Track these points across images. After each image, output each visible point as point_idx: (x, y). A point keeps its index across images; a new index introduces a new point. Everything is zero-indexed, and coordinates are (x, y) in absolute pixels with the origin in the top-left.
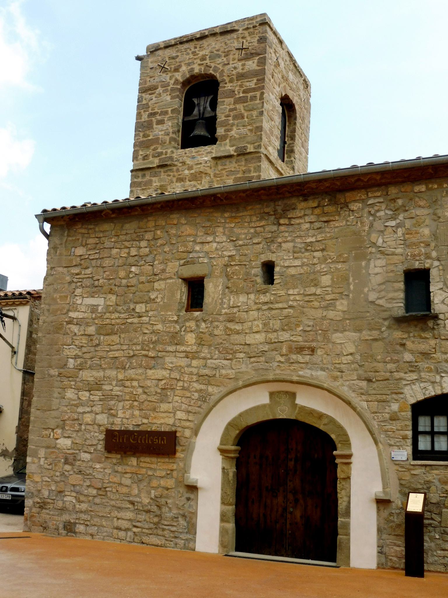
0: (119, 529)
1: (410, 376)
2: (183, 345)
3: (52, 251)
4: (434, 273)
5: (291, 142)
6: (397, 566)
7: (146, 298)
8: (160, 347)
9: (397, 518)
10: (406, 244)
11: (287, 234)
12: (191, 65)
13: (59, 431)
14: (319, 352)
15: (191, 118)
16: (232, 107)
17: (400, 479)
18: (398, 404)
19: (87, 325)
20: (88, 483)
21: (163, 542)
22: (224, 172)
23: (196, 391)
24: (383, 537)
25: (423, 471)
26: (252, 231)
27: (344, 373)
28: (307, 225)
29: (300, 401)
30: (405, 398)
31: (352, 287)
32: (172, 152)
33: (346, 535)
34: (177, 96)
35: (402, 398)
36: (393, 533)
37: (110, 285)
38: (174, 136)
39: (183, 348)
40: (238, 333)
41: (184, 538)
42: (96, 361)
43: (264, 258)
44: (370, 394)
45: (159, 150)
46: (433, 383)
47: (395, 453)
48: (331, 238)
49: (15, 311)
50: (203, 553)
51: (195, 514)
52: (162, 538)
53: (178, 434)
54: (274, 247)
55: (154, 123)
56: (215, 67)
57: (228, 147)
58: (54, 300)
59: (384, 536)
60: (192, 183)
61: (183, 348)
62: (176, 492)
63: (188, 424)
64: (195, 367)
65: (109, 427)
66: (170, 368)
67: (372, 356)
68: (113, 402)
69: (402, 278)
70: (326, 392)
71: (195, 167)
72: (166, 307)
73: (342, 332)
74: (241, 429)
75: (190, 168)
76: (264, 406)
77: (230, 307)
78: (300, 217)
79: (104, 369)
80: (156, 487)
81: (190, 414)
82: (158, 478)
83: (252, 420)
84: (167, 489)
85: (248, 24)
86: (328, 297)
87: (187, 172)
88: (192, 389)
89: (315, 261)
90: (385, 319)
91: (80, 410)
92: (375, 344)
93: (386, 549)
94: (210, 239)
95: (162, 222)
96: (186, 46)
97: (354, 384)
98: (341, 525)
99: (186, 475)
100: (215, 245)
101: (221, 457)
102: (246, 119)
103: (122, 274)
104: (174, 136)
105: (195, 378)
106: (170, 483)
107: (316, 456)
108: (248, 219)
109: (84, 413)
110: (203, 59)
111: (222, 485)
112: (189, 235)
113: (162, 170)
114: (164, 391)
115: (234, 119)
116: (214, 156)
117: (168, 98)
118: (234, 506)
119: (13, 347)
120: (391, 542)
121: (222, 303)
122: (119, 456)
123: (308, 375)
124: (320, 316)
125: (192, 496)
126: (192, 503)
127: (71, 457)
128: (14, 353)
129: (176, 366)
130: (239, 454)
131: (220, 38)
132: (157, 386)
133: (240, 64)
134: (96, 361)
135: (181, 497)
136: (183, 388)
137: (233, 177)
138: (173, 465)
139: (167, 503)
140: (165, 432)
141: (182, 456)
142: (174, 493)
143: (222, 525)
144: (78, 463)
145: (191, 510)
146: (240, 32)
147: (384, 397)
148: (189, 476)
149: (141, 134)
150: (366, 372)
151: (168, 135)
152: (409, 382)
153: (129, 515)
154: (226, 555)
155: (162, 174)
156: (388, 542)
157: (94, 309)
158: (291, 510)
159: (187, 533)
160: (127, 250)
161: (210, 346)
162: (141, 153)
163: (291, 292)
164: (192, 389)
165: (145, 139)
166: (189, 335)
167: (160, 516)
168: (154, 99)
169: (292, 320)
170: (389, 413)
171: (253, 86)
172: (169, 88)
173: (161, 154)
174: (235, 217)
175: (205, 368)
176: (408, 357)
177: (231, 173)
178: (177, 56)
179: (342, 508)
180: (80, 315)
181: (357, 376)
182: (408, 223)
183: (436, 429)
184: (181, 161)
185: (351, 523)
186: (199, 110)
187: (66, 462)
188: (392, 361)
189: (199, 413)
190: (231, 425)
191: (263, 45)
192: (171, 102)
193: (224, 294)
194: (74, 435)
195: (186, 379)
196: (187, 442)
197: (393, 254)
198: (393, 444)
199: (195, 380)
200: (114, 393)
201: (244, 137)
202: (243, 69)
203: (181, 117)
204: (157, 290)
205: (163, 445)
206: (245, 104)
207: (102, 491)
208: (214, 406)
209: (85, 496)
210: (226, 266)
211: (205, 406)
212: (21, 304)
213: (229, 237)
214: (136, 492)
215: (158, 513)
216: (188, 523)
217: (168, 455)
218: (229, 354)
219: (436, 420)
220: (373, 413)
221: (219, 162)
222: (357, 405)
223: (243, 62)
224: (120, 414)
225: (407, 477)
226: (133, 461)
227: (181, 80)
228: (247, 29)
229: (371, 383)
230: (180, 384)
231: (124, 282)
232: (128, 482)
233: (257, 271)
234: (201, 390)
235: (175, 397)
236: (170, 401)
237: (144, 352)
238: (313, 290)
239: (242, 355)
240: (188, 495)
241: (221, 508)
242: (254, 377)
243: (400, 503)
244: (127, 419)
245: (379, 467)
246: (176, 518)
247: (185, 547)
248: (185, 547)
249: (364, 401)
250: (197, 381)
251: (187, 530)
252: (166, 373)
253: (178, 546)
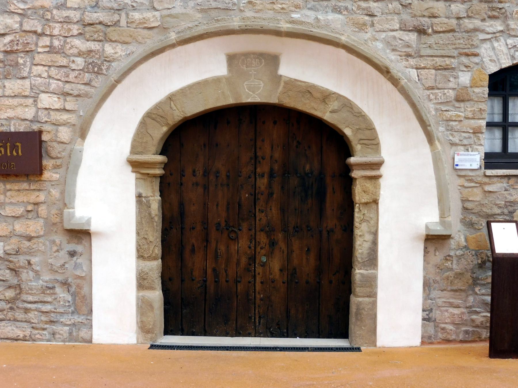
1: (491, 26)
6: (454, 337)
9: (458, 264)
18: (470, 73)
21: (28, 332)
23: (80, 54)
24: (432, 296)
25: (505, 185)
27: (376, 18)
29: (286, 70)
33: (369, 296)
35: (477, 64)
36: (449, 288)
41: (69, 323)
44: (421, 56)
47: (460, 157)
50: (109, 346)
51: (88, 279)
52: (25, 325)
53: (45, 137)
59: (435, 294)
62: (48, 243)
63: (65, 117)
64: (75, 9)
66: (20, 11)
70: (343, 52)
74: (171, 123)
76: (217, 80)
80: (6, 236)
81: (68, 98)
82: (10, 220)
83: (194, 107)
84: (30, 238)
88: (71, 51)
93: (436, 314)
97: (394, 38)
98: (361, 281)
99: (66, 211)
101: (133, 176)
105: (75, 29)
106: (35, 227)
107: (308, 167)
111: (137, 226)
114: (11, 57)
118: (160, 260)
120: (445, 302)
123: (311, 20)
125: (79, 248)
126: (79, 261)
129: (34, 8)
130: (164, 169)
135: (58, 251)
136: (51, 50)
138: (37, 193)
139: (29, 263)
141: (56, 176)
142: (44, 244)
143: (141, 294)
145: (78, 273)
147: (448, 61)
148: (74, 213)
150: (415, 16)
152: (489, 36)
154: (152, 347)
156: (440, 302)
158: (264, 259)
159: (73, 313)
164: (71, 51)
167: (18, 287)
170: (454, 89)
175: (96, 9)
179: (362, 253)
181: (400, 23)
185: (379, 276)
189: (87, 95)
190: (151, 116)
195: (56, 32)
196: (64, 150)
198: (457, 141)
199: (75, 32)
208: (118, 81)
215: (15, 281)
216: (74, 295)
217: (27, 175)
220: (428, 89)
222: (400, 74)
225: (477, 195)
229: (423, 37)
230: (46, 41)
234: (91, 51)
235: (35, 68)
236: (25, 74)
240: (72, 247)
241: (138, 266)
243: (463, 239)
245: (434, 182)
246: (50, 288)
247: (71, 338)
248: (71, 338)
249: (413, 68)
250: (80, 34)
251: (72, 308)
252: (13, 22)
253: (57, 336)
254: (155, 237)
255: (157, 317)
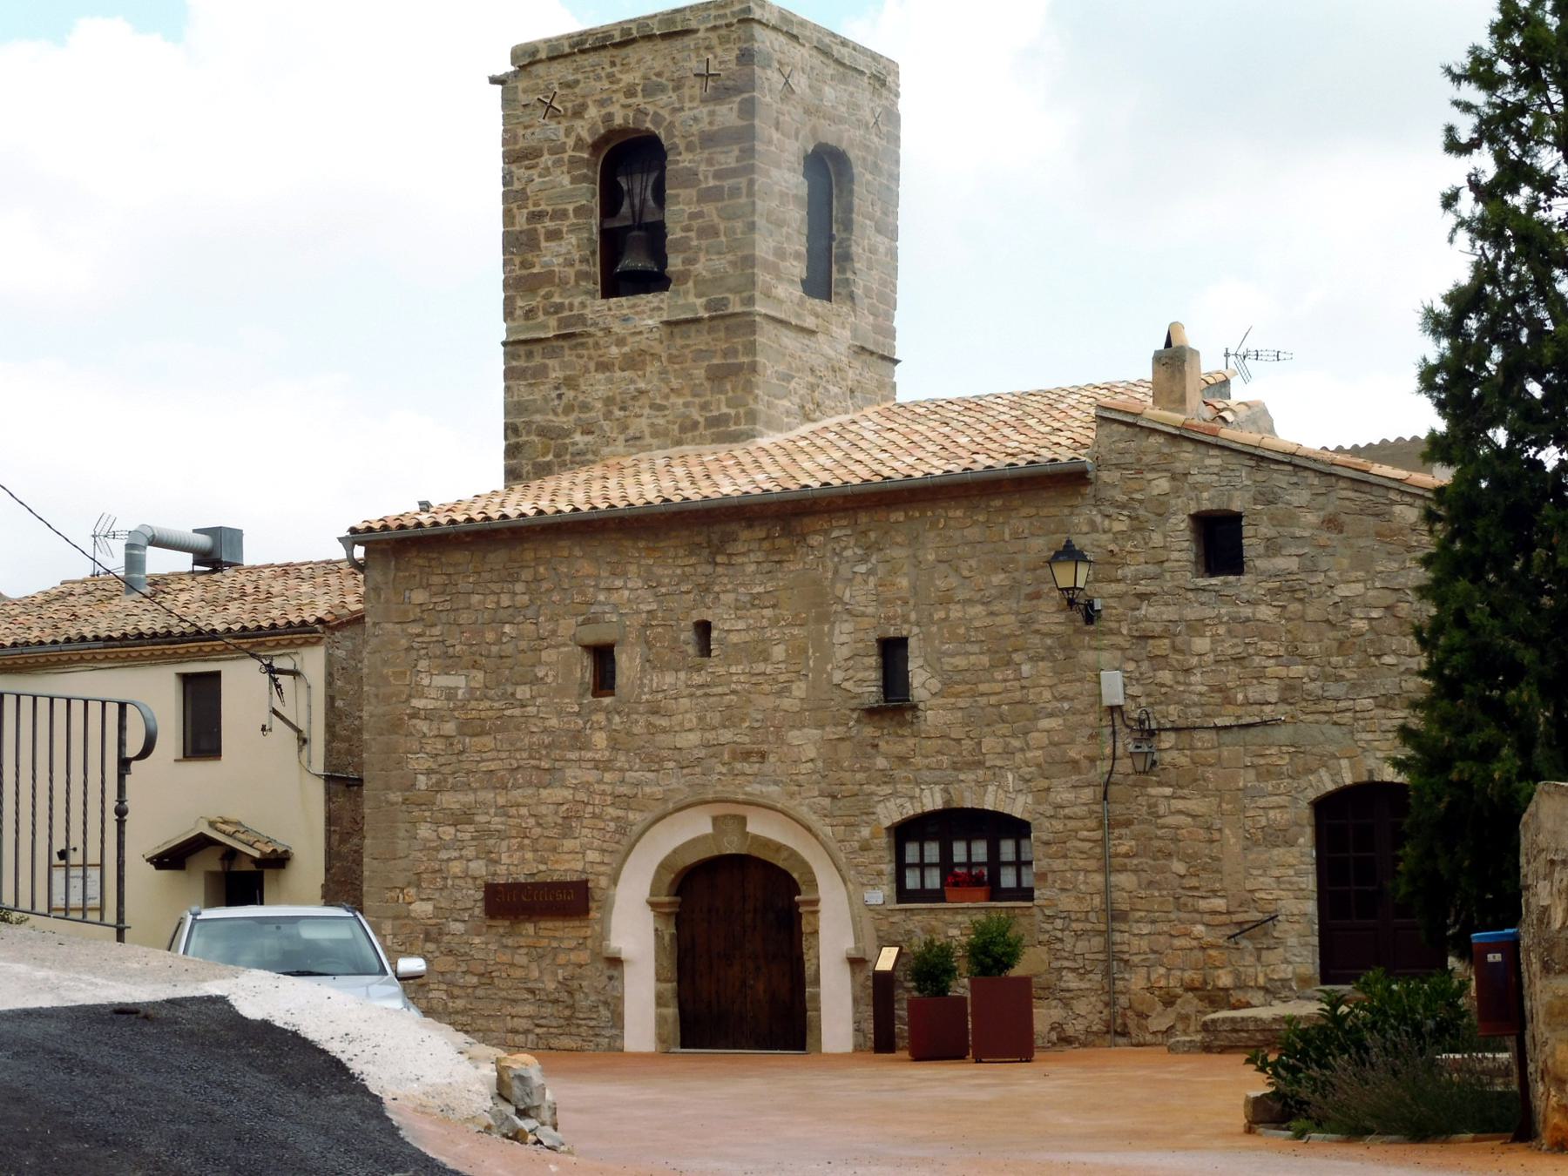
0: (515, 1031)
2: (590, 750)
3: (372, 595)
4: (912, 643)
5: (844, 235)
7: (530, 677)
8: (556, 753)
10: (882, 602)
11: (726, 580)
12: (610, 104)
13: (412, 891)
14: (772, 758)
15: (616, 223)
16: (694, 209)
17: (878, 930)
19: (442, 719)
20: (464, 968)
22: (687, 351)
26: (679, 571)
28: (753, 568)
30: (877, 820)
31: (811, 663)
32: (583, 305)
34: (585, 178)
37: (473, 654)
38: (584, 267)
39: (589, 755)
40: (664, 731)
42: (461, 777)
43: (696, 616)
45: (557, 299)
46: (912, 798)
48: (786, 588)
49: (296, 658)
51: (621, 999)
53: (590, 885)
54: (709, 599)
55: (542, 238)
56: (656, 113)
57: (692, 299)
58: (385, 678)
60: (626, 374)
61: (589, 755)
63: (603, 869)
65: (490, 879)
67: (837, 762)
68: (492, 841)
69: (875, 650)
71: (630, 340)
72: (561, 691)
73: (800, 729)
75: (621, 342)
76: (705, 838)
77: (652, 692)
78: (743, 554)
79: (475, 790)
84: (580, 966)
85: (716, 18)
86: (782, 678)
87: (614, 350)
89: (765, 622)
90: (853, 710)
91: (444, 855)
92: (842, 745)
94: (619, 583)
95: (545, 553)
96: (592, 58)
100: (627, 593)
102: (723, 239)
103: (490, 636)
104: (584, 267)
105: (609, 799)
106: (584, 956)
108: (671, 553)
109: (449, 860)
110: (630, 92)
112: (588, 576)
113: (564, 343)
115: (699, 237)
116: (665, 318)
117: (566, 180)
119: (299, 731)
121: (642, 686)
122: (507, 923)
124: (771, 705)
125: (615, 973)
127: (434, 930)
128: (303, 741)
131: (662, 46)
132: (556, 813)
133: (705, 110)
134: (461, 777)
136: (594, 816)
137: (706, 364)
140: (571, 883)
144: (446, 939)
146: (701, 34)
149: (517, 260)
151: (572, 265)
153: (528, 1009)
155: (567, 352)
157: (450, 693)
160: (493, 598)
161: (628, 751)
162: (520, 303)
163: (733, 670)
165: (525, 272)
166: (598, 734)
167: (572, 1007)
168: (537, 180)
169: (735, 712)
171: (733, 165)
172: (566, 156)
173: (559, 308)
174: (654, 549)
176: (881, 763)
177: (700, 355)
178: (577, 82)
180: (431, 704)
182: (881, 570)
183: (927, 860)
184: (602, 325)
186: (632, 206)
187: (428, 938)
188: (862, 769)
190: (663, 866)
191: (747, 70)
192: (572, 190)
193: (643, 670)
194: (437, 895)
197: (863, 615)
200: (493, 827)
201: (722, 278)
202: (711, 123)
203: (595, 222)
204: (547, 664)
205: (570, 901)
206: (720, 205)
207: (487, 977)
208: (637, 841)
209: (461, 987)
210: (645, 626)
211: (625, 841)
212: (307, 643)
213: (646, 581)
214: (536, 974)
216: (613, 1012)
218: (654, 762)
219: (927, 846)
221: (676, 330)
223: (711, 107)
224: (505, 859)
226: (529, 928)
227: (590, 141)
228: (715, 28)
230: (590, 809)
231: (495, 649)
232: (524, 960)
233: (688, 635)
237: (533, 762)
238: (760, 667)
239: (671, 764)
240: (608, 972)
242: (684, 795)
244: (516, 865)
248: (610, 1048)
252: (568, 794)
254: (670, 965)
255: (673, 1029)
